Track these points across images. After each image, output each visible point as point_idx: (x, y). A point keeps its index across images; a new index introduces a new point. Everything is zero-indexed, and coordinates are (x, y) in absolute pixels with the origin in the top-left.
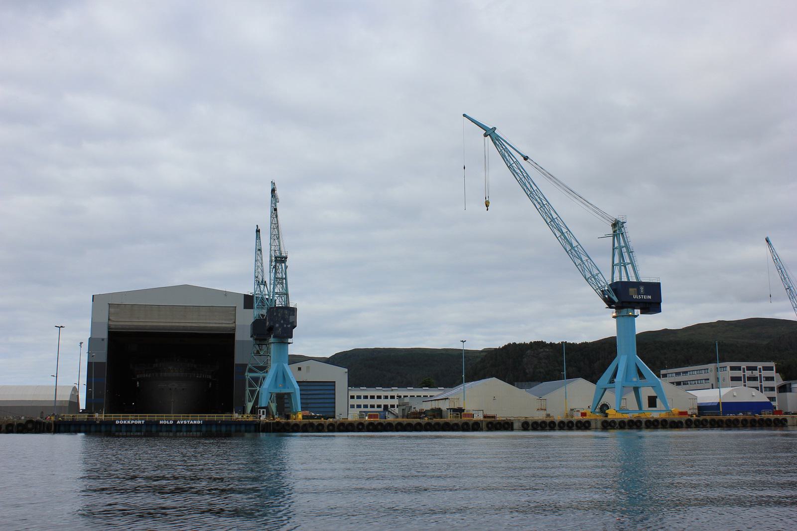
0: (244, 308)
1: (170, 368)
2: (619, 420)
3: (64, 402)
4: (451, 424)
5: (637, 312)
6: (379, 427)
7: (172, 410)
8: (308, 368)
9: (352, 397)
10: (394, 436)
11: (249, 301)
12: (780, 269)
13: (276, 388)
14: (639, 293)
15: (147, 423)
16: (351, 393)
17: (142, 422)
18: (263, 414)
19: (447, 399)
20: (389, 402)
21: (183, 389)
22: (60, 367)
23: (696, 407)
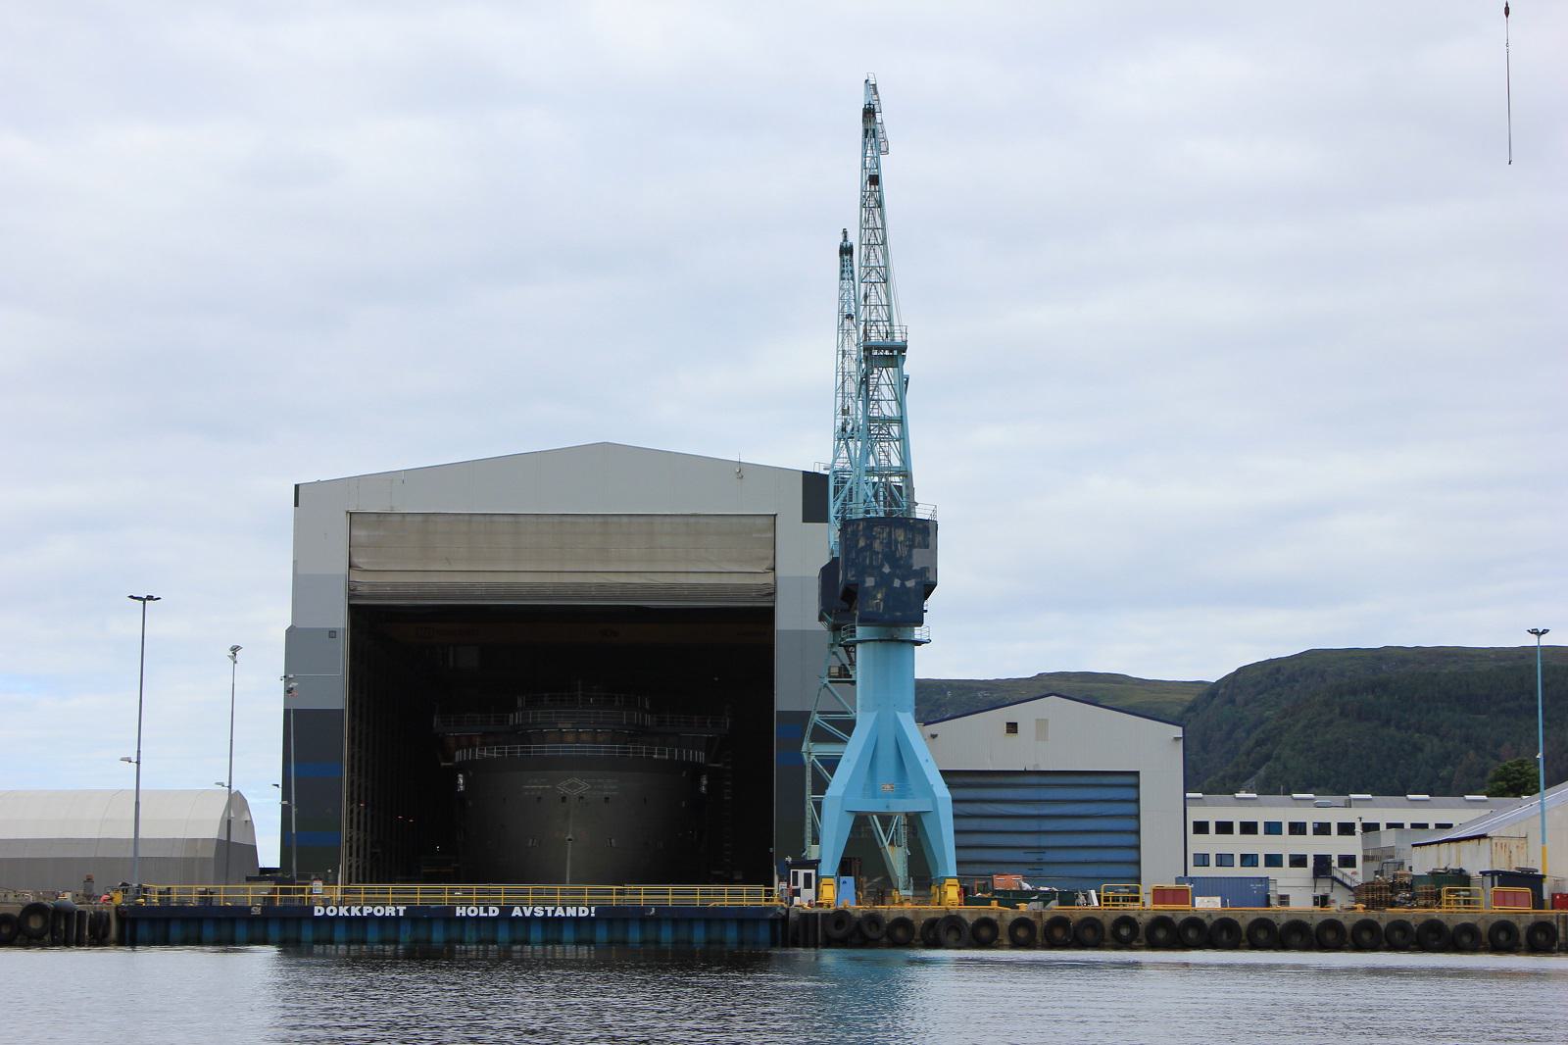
0: (804, 521)
1: (566, 727)
3: (199, 844)
4: (1451, 926)
6: (1191, 934)
7: (568, 872)
8: (1042, 725)
9: (1201, 828)
10: (1279, 966)
11: (815, 489)
12: (903, 641)
13: (874, 796)
15: (416, 916)
16: (1196, 814)
17: (397, 911)
18: (808, 885)
19: (1484, 836)
20: (1334, 846)
22: (196, 727)
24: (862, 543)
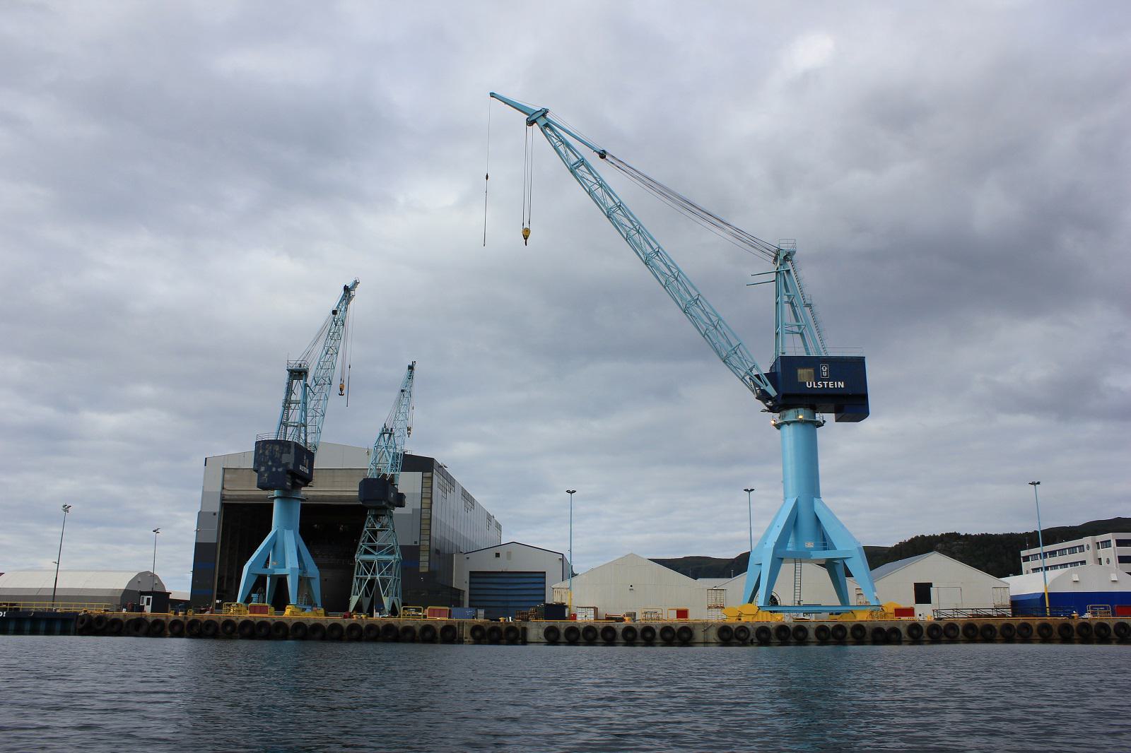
2: (583, 627)
4: (886, 628)
5: (830, 417)
14: (818, 377)
21: (326, 580)
23: (1008, 603)
24: (261, 452)
